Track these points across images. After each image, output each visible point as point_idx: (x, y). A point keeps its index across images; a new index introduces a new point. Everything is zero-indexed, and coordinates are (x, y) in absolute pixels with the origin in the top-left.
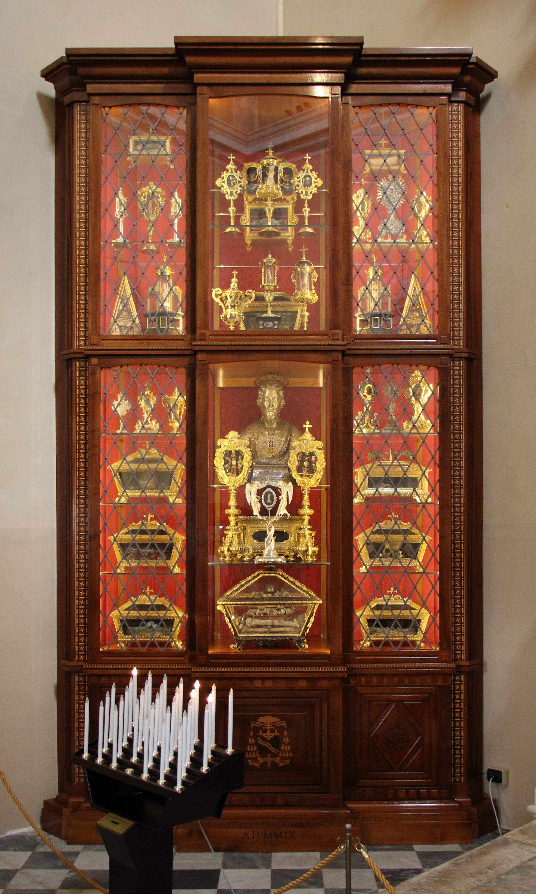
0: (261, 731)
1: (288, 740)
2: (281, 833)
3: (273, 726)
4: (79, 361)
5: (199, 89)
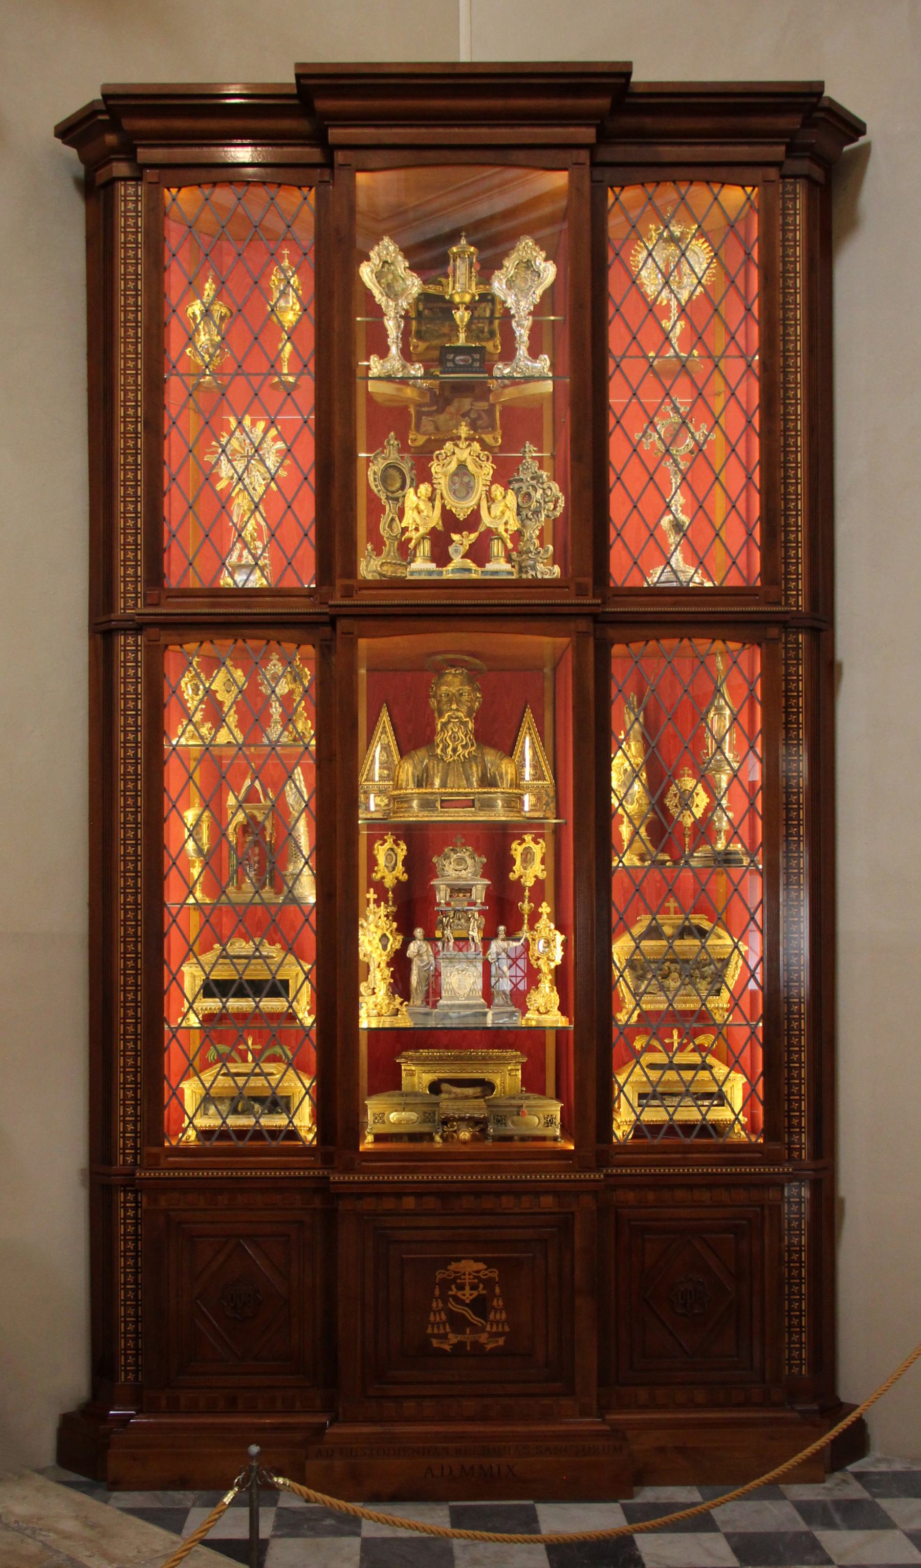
0: (453, 1287)
1: (501, 1303)
2: (472, 1467)
3: (475, 1277)
4: (125, 635)
5: (340, 157)
